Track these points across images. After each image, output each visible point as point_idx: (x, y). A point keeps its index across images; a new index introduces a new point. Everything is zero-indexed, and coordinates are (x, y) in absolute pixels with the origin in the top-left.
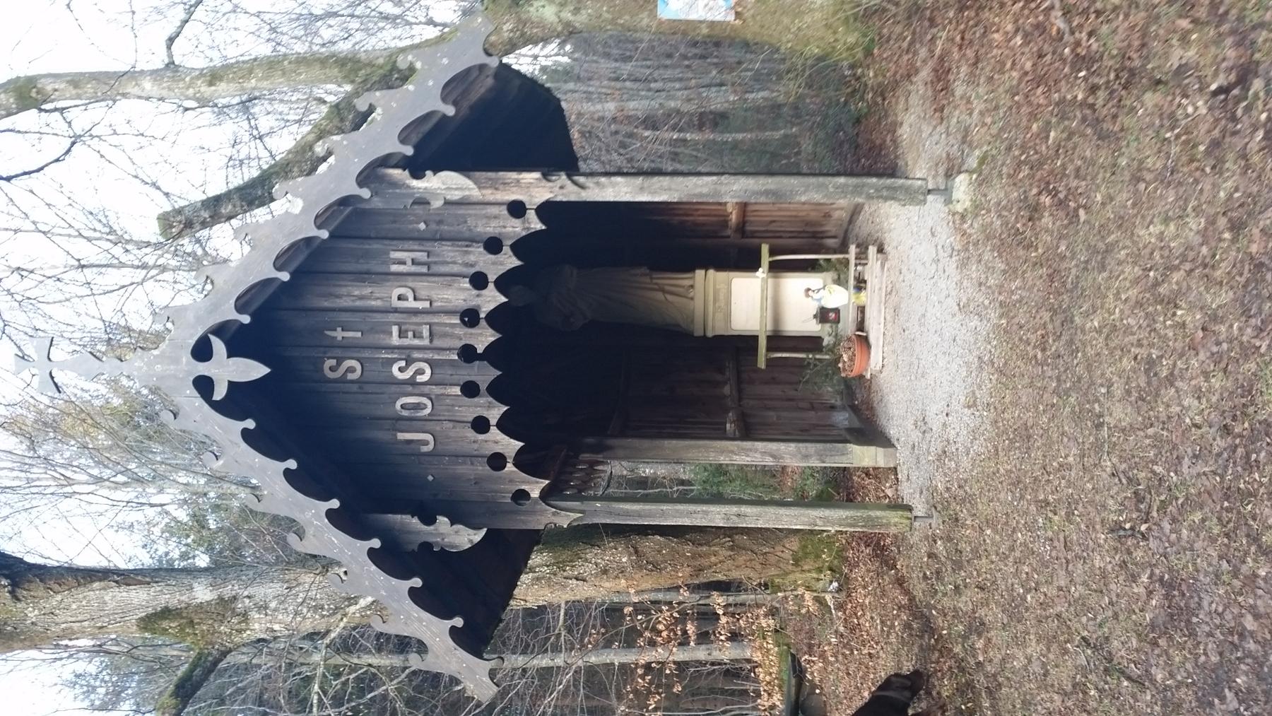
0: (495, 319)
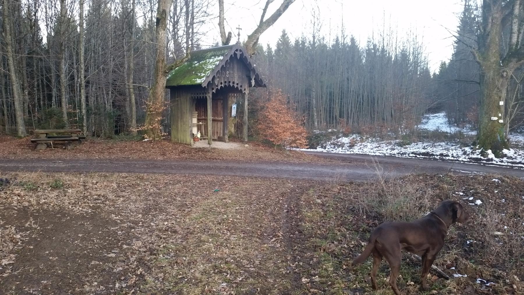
0: (233, 86)
